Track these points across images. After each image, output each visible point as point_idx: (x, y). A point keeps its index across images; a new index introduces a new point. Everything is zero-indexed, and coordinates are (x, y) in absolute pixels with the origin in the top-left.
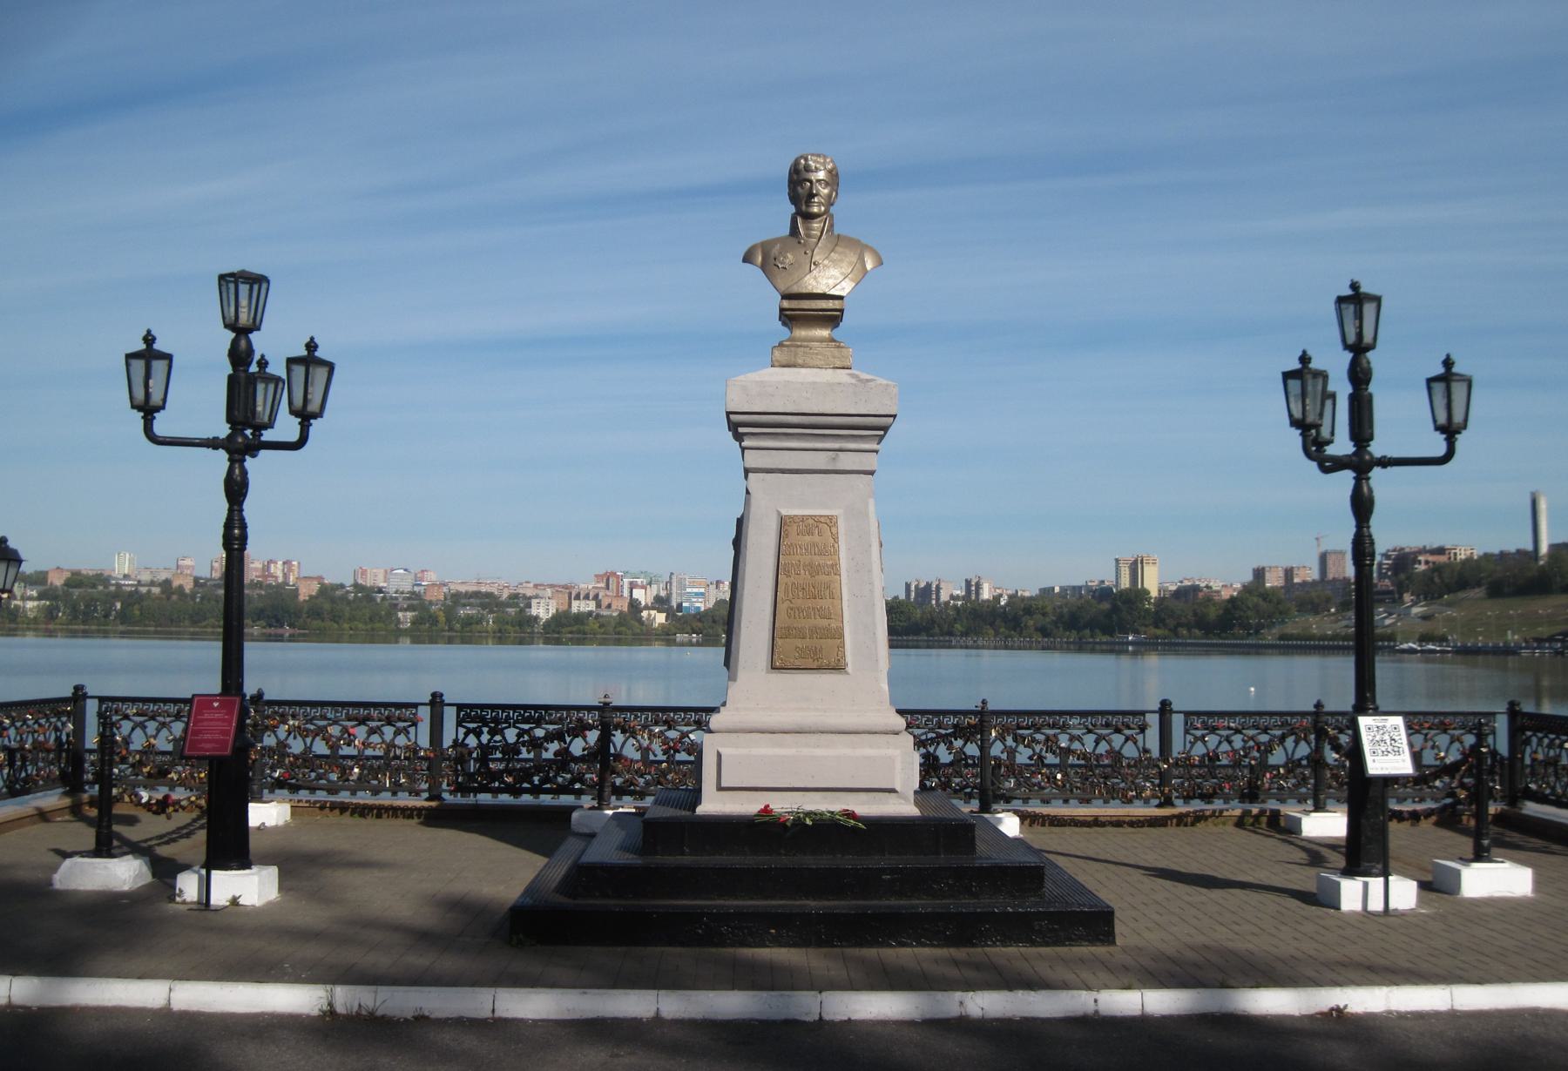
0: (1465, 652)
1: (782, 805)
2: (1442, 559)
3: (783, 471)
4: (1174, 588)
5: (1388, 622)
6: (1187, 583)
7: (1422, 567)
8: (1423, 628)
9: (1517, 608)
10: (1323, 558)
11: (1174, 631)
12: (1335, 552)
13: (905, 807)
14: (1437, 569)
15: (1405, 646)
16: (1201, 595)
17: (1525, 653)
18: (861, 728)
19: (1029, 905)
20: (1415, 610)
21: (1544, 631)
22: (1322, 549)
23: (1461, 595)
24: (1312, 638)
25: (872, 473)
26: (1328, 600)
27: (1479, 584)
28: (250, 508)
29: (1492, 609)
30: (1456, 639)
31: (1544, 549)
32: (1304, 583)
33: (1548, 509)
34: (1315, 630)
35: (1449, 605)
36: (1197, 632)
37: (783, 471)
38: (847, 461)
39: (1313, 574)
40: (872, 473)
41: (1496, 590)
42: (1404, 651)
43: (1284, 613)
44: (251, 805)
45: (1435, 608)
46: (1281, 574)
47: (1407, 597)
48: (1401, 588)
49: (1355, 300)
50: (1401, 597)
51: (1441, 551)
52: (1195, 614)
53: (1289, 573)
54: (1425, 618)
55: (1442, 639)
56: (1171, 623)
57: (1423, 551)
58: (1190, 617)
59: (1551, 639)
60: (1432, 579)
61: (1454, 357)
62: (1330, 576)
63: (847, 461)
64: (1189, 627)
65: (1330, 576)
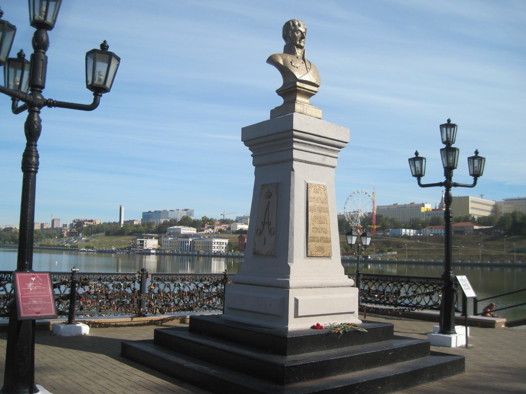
0: (100, 252)
1: (325, 322)
2: (92, 223)
3: (306, 162)
4: (4, 228)
5: (75, 242)
6: (8, 227)
7: (85, 226)
8: (87, 244)
9: (115, 239)
10: (53, 221)
11: (4, 242)
12: (57, 219)
13: (355, 320)
14: (90, 226)
15: (82, 250)
16: (13, 231)
17: (118, 253)
18: (335, 285)
19: (429, 361)
20: (83, 239)
21: (123, 246)
22: (53, 218)
23: (97, 234)
24: (44, 245)
25: (333, 167)
26: (55, 234)
27: (103, 232)
28: (41, 143)
29: (108, 239)
30: (96, 248)
31: (122, 223)
32: (47, 229)
33: (125, 211)
34: (51, 243)
35: (94, 237)
36: (12, 242)
37: (306, 162)
38: (329, 161)
39: (50, 226)
40: (333, 167)
41: (108, 234)
42: (82, 251)
43: (41, 238)
44: (153, 338)
45: (89, 238)
46: (40, 225)
47: (80, 234)
48: (79, 232)
49: (449, 126)
50: (79, 234)
51: (91, 221)
52: (12, 237)
53: (42, 225)
54: (86, 241)
55: (92, 248)
56: (3, 239)
57: (86, 221)
58: (10, 238)
59: (125, 249)
60: (88, 229)
61: (479, 151)
62: (55, 227)
63: (329, 161)
64: (9, 241)
65: (55, 227)
